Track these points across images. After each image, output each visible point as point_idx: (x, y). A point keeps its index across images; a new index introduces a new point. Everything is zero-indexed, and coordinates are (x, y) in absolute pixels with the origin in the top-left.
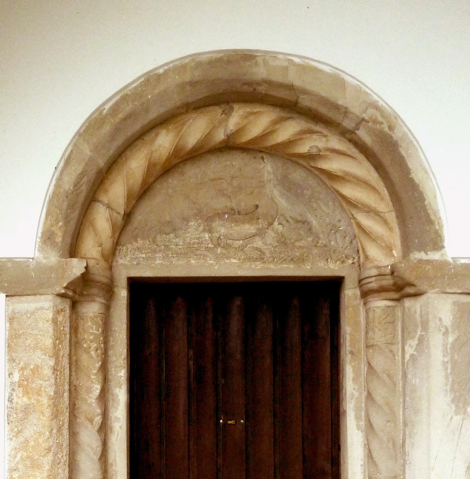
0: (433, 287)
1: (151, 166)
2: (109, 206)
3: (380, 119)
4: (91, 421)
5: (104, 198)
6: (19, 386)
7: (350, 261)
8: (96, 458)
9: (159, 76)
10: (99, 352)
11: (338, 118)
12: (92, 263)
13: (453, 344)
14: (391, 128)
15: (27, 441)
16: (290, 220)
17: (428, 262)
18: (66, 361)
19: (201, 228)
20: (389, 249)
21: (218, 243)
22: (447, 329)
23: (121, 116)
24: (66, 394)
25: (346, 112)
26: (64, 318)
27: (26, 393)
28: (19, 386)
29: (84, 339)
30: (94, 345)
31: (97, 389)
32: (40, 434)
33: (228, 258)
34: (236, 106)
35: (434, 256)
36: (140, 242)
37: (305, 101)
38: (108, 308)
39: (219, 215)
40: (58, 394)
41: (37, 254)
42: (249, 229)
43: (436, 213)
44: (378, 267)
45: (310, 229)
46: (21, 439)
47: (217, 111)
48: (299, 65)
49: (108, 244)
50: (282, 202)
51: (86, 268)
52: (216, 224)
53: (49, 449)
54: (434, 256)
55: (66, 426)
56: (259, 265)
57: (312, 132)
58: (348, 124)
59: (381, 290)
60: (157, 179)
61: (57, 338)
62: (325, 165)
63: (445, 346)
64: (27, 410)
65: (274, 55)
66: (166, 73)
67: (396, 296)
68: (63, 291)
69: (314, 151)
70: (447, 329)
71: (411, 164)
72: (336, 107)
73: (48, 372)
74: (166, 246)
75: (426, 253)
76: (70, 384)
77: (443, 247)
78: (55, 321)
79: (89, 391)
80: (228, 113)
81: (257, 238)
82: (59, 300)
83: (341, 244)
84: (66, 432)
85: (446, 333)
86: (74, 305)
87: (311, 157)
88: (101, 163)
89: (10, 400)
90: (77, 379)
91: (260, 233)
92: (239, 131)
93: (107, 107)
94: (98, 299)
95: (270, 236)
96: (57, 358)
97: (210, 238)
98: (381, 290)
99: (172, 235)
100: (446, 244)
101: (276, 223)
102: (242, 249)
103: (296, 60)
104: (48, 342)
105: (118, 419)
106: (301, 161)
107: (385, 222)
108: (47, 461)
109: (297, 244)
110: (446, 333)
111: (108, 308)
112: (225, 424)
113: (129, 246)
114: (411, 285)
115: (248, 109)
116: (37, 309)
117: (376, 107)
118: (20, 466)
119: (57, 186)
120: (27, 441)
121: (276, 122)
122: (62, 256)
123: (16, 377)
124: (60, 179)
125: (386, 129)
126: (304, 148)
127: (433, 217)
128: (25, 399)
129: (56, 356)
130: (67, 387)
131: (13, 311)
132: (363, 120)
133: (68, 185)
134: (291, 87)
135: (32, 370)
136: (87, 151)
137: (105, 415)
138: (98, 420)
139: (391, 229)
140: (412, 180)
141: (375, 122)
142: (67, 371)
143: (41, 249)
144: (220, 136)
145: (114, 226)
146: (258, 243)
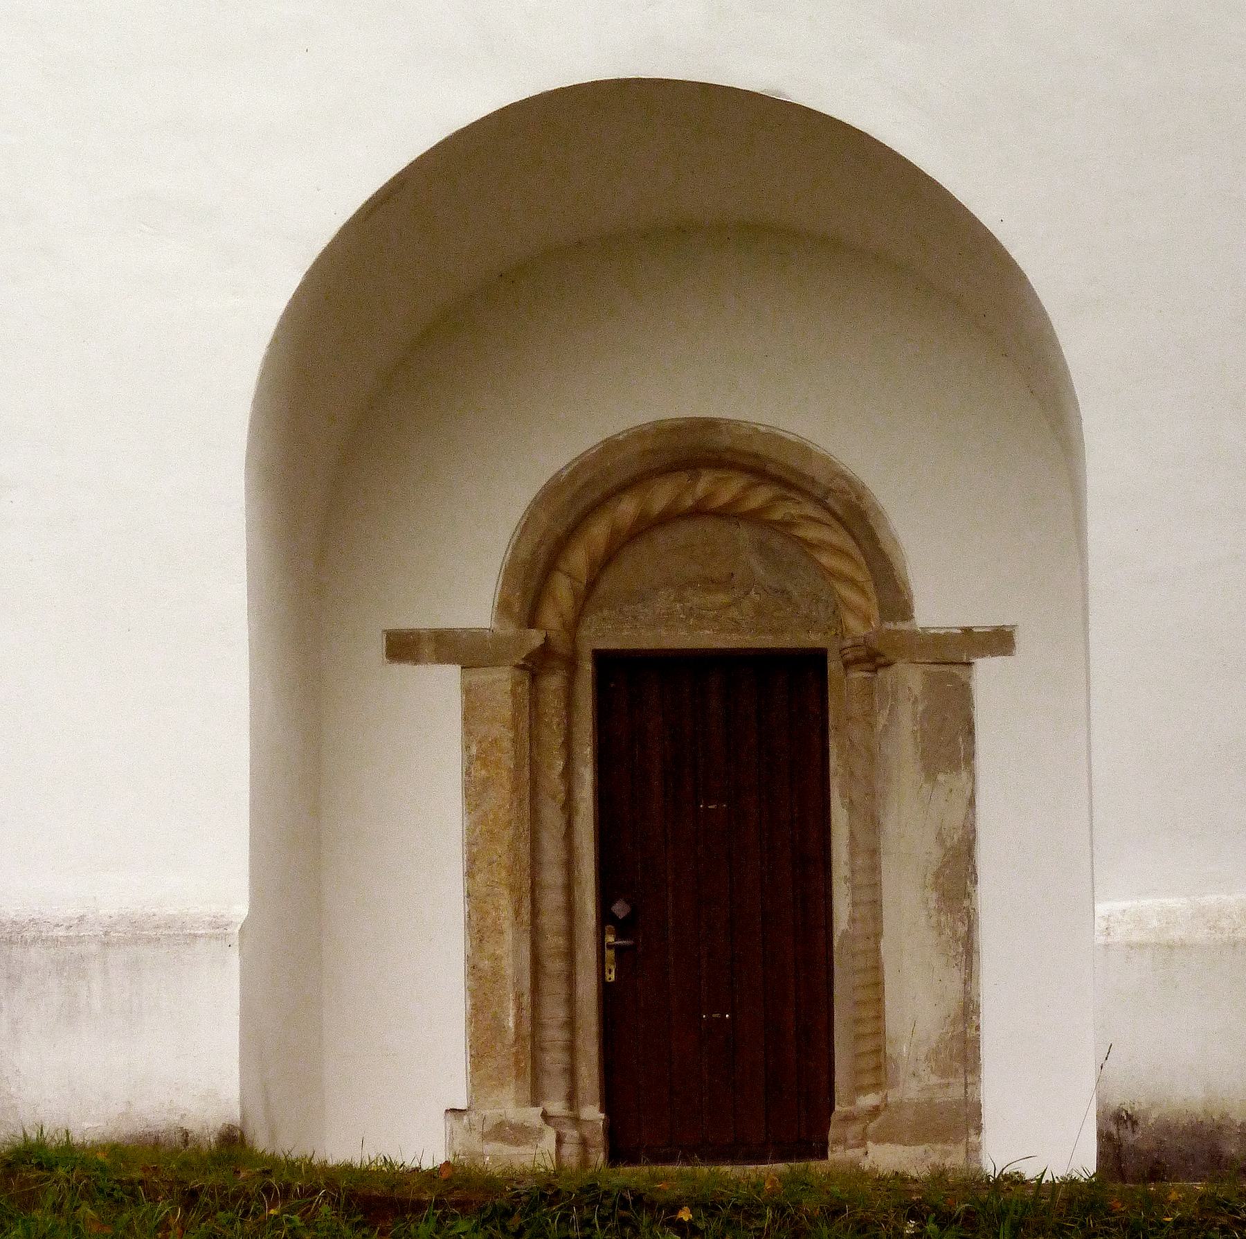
0: (902, 656)
1: (615, 532)
2: (569, 575)
3: (848, 489)
4: (554, 798)
5: (563, 565)
6: (477, 760)
7: (833, 633)
8: (560, 836)
9: (618, 443)
10: (562, 726)
11: (808, 487)
12: (552, 635)
13: (924, 711)
14: (859, 498)
15: (486, 814)
16: (769, 591)
17: (897, 632)
18: (526, 735)
19: (672, 598)
20: (867, 619)
21: (690, 612)
22: (916, 698)
23: (579, 483)
24: (527, 768)
25: (813, 481)
26: (523, 689)
27: (485, 765)
28: (477, 760)
29: (545, 713)
30: (556, 720)
31: (560, 764)
32: (500, 807)
33: (701, 629)
34: (704, 472)
35: (903, 626)
36: (606, 613)
37: (771, 468)
38: (571, 682)
39: (691, 583)
40: (518, 767)
41: (494, 625)
42: (722, 598)
43: (906, 583)
44: (854, 638)
45: (789, 599)
46: (480, 813)
47: (684, 477)
48: (763, 434)
49: (570, 616)
50: (760, 571)
51: (546, 639)
52: (689, 593)
53: (510, 823)
54: (903, 626)
55: (527, 801)
56: (735, 636)
57: (785, 499)
58: (818, 493)
59: (857, 661)
60: (623, 545)
61: (517, 709)
62: (799, 533)
63: (914, 714)
64: (486, 783)
65: (738, 424)
66: (626, 440)
67: (868, 666)
68: (522, 663)
69: (788, 518)
70: (916, 698)
71: (881, 534)
72: (804, 477)
73: (507, 744)
74: (635, 617)
75: (895, 624)
76: (531, 758)
77: (912, 617)
78: (513, 693)
79: (550, 767)
80: (695, 478)
81: (733, 608)
82: (517, 672)
83: (822, 614)
84: (527, 807)
85: (915, 702)
86: (534, 678)
87: (788, 524)
88: (560, 531)
89: (468, 773)
90: (539, 754)
91: (735, 603)
92: (709, 497)
93: (565, 473)
94: (561, 673)
95: (746, 604)
96: (517, 731)
97: (681, 607)
98: (857, 661)
99: (640, 605)
100: (916, 614)
101: (753, 593)
102: (716, 619)
103: (762, 429)
104: (507, 713)
105: (583, 799)
106: (779, 528)
107: (863, 592)
108: (508, 834)
109: (776, 614)
110: (915, 702)
111: (571, 682)
112: (706, 809)
113: (594, 617)
114: (880, 655)
115: (720, 474)
116: (494, 682)
117: (843, 476)
118: (480, 841)
119: (514, 555)
120: (486, 814)
121: (745, 489)
122: (520, 626)
123: (474, 750)
124: (515, 548)
125: (854, 499)
126: (777, 515)
127: (901, 586)
128: (483, 772)
129: (515, 727)
130: (527, 760)
131: (470, 683)
132: (831, 490)
133: (524, 554)
134: (756, 456)
135: (491, 743)
136: (543, 517)
137: (570, 793)
138: (561, 796)
139: (869, 599)
140: (880, 549)
141: (842, 492)
142: (527, 745)
143: (498, 620)
144: (689, 502)
145: (576, 596)
146: (734, 613)
